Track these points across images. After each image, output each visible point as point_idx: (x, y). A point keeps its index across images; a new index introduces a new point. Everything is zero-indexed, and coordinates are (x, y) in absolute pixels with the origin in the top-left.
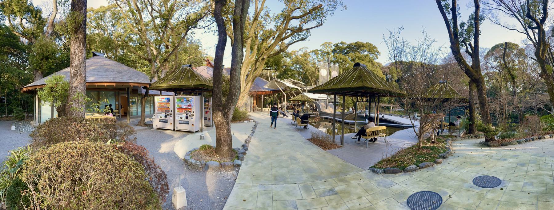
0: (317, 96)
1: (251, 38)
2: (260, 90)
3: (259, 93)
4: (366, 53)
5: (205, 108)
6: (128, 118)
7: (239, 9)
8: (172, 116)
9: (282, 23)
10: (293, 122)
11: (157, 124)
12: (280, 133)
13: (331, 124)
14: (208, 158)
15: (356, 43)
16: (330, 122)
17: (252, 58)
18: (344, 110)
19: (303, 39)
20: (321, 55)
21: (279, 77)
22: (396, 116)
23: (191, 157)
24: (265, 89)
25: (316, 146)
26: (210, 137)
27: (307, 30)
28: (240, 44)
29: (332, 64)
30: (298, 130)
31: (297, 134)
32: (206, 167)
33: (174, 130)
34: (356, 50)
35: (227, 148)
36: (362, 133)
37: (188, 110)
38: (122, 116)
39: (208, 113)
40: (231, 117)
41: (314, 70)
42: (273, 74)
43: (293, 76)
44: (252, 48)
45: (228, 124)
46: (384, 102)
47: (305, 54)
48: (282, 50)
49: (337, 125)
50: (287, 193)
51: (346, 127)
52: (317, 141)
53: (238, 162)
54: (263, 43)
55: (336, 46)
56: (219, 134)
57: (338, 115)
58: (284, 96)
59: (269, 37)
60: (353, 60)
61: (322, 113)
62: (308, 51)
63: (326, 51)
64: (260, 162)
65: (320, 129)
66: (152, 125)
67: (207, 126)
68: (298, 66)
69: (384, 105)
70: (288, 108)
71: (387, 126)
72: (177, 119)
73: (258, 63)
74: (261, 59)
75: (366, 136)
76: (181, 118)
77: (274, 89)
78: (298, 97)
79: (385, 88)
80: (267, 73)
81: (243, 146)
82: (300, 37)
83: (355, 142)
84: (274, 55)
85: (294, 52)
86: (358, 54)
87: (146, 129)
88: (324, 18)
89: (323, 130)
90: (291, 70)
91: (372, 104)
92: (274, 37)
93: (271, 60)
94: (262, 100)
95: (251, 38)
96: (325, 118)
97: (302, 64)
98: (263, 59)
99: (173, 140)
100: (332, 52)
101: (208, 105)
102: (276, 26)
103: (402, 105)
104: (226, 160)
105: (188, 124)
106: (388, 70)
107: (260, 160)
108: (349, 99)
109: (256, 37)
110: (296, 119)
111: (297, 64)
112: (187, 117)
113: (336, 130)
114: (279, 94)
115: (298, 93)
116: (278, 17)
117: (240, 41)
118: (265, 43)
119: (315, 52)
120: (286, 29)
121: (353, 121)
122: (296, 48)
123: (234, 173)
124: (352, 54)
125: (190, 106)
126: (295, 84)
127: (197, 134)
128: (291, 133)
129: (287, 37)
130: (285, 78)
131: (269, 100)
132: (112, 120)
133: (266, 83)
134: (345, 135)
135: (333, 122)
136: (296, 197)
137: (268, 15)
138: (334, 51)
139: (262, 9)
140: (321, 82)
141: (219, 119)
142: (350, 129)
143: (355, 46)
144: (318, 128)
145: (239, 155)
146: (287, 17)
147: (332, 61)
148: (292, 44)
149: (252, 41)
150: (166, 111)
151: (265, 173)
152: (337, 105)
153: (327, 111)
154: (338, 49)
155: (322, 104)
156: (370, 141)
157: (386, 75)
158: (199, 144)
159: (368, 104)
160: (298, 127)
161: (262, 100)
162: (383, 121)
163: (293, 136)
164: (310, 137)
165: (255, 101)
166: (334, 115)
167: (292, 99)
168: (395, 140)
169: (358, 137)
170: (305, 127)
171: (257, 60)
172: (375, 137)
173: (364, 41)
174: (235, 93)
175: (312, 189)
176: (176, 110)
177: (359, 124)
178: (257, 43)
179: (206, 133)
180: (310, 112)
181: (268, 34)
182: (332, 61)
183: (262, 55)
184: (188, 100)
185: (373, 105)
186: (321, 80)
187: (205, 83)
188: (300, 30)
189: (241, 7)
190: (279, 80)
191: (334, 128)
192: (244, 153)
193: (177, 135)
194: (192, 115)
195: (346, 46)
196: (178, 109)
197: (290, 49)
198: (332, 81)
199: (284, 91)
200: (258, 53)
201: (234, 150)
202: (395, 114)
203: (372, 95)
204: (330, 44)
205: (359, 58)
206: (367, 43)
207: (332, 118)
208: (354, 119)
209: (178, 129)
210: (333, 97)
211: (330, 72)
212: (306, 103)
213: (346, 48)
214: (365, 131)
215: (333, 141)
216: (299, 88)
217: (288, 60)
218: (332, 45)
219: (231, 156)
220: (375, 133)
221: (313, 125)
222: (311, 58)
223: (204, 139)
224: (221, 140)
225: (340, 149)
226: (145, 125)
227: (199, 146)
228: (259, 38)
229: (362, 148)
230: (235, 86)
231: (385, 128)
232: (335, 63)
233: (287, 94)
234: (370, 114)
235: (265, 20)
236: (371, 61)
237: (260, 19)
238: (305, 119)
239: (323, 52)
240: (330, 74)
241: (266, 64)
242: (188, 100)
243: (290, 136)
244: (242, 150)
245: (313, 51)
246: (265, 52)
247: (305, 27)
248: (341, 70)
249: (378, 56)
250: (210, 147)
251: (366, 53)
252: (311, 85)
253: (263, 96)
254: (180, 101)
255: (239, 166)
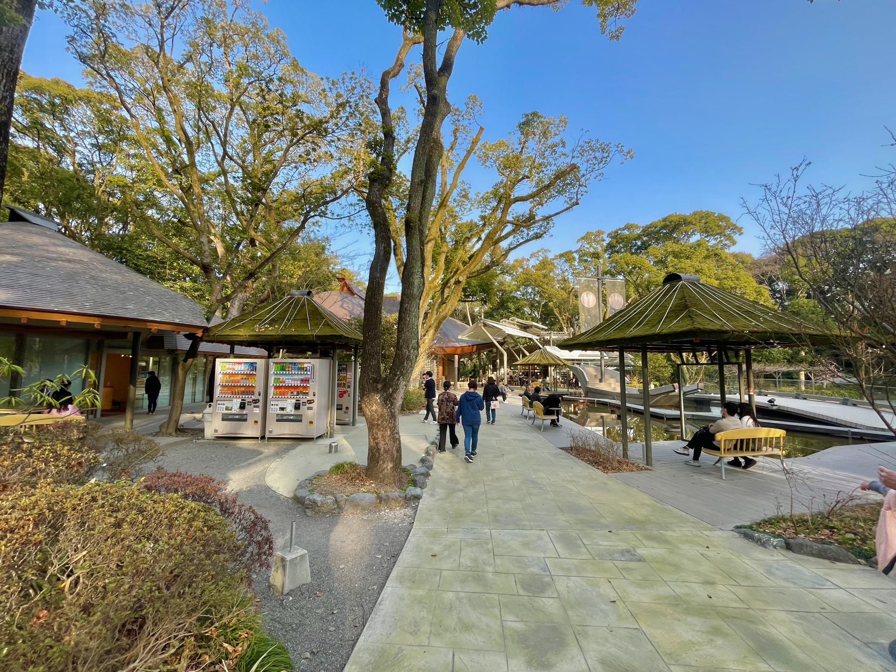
0: (576, 354)
1: (433, 242)
2: (451, 344)
3: (448, 351)
4: (695, 239)
5: (339, 385)
6: (129, 415)
7: (417, 201)
8: (260, 404)
9: (494, 210)
10: (526, 411)
11: (214, 426)
12: (498, 436)
13: (614, 416)
14: (350, 489)
15: (664, 220)
16: (613, 412)
17: (434, 279)
18: (646, 385)
19: (538, 236)
20: (581, 261)
21: (489, 315)
22: (823, 400)
23: (312, 492)
24: (462, 341)
25: (584, 463)
26: (353, 447)
27: (547, 218)
28: (419, 264)
29: (608, 279)
30: (539, 428)
31: (537, 438)
32: (336, 512)
33: (263, 438)
34: (668, 237)
35: (390, 465)
36: (704, 440)
37: (301, 390)
38: (105, 413)
39: (346, 395)
40: (399, 402)
41: (565, 295)
42: (477, 309)
43: (518, 311)
44: (435, 261)
45: (393, 416)
46: (770, 360)
47: (544, 264)
48: (494, 263)
49: (632, 420)
50: (526, 545)
51: (655, 424)
52: (581, 451)
53: (413, 491)
54: (456, 249)
55: (615, 236)
56: (375, 439)
57: (632, 396)
58: (502, 355)
59: (468, 239)
60: (661, 262)
61: (589, 392)
62: (551, 256)
63: (592, 250)
64: (461, 491)
65: (589, 428)
66: (203, 430)
67: (341, 423)
68: (530, 290)
69: (770, 368)
70: (511, 381)
71: (788, 429)
72: (274, 410)
73: (447, 291)
74: (453, 281)
75: (718, 449)
76: (282, 409)
77: (480, 341)
78: (533, 357)
79: (763, 327)
80: (465, 308)
81: (423, 461)
82: (531, 233)
83: (687, 463)
84: (479, 273)
85: (520, 263)
86: (670, 246)
87: (182, 442)
88: (582, 189)
89: (599, 430)
90: (515, 300)
91: (726, 368)
92: (480, 239)
93: (474, 282)
94: (456, 365)
95: (433, 242)
96: (599, 403)
97: (539, 286)
98: (458, 282)
99: (260, 460)
100: (606, 251)
101: (345, 378)
102: (483, 218)
103: (849, 366)
104: (389, 489)
105: (301, 421)
106: (775, 270)
107: (460, 487)
108: (657, 359)
109: (443, 239)
110: (531, 405)
111: (527, 286)
112: (297, 407)
113: (631, 433)
114: (491, 351)
115: (532, 348)
116: (486, 199)
117: (419, 258)
118: (461, 252)
119: (567, 256)
120: (503, 223)
121: (677, 413)
122: (524, 255)
123: (409, 511)
124: (657, 249)
125: (307, 381)
126: (525, 328)
127: (321, 442)
128: (523, 436)
129: (506, 237)
130: (502, 317)
131: (470, 365)
132: (78, 425)
133: (462, 330)
134: (654, 443)
135: (622, 412)
136: (545, 552)
137: (465, 196)
138: (610, 246)
139: (454, 186)
140: (586, 324)
141: (374, 408)
142: (666, 431)
143: (664, 227)
144: (584, 424)
145: (417, 478)
146: (504, 199)
147: (606, 273)
148: (515, 248)
149: (436, 245)
150: (243, 393)
151: (474, 511)
152: (629, 372)
153: (603, 387)
154: (619, 243)
155: (589, 372)
156: (730, 463)
157: (771, 282)
158: (327, 463)
159: (716, 367)
160: (537, 422)
161: (456, 365)
162: (768, 414)
163: (527, 441)
164: (568, 443)
165: (441, 368)
166: (623, 395)
167: (520, 360)
168: (820, 470)
169: (692, 451)
170: (554, 423)
171: (445, 284)
172: (749, 455)
173: (685, 210)
174: (409, 357)
175: (580, 542)
176: (271, 391)
177: (692, 420)
178: (445, 249)
179: (340, 439)
180: (562, 389)
181: (465, 230)
182: (606, 273)
183: (456, 273)
184: (302, 369)
185: (730, 371)
186: (582, 317)
187: (341, 333)
188: (530, 220)
189: (420, 198)
190: (490, 322)
191: (625, 427)
192: (427, 475)
193: (269, 449)
194: (310, 402)
195: (638, 232)
196: (276, 387)
197: (511, 258)
198: (608, 323)
199: (501, 344)
200: (447, 269)
201: (404, 470)
202: (820, 394)
203: (726, 347)
204: (600, 233)
205: (676, 255)
206: (695, 214)
207: (618, 402)
208: (678, 407)
209: (273, 435)
210: (616, 354)
211: (604, 296)
212: (551, 369)
213: (639, 237)
214: (712, 436)
215: (625, 455)
216: (535, 338)
217: (508, 278)
218: (605, 236)
219: (400, 481)
220: (741, 444)
221: (571, 419)
222: (558, 272)
223: (336, 451)
224: (379, 449)
225: (645, 474)
226: (181, 430)
227: (327, 467)
228: (448, 240)
229: (706, 479)
230: (407, 342)
231: (780, 433)
232: (613, 275)
233: (507, 350)
234: (723, 394)
235: (460, 205)
236: (715, 255)
237: (451, 203)
238: (552, 404)
239: (582, 254)
240: (605, 302)
241: (464, 290)
242: (302, 369)
243: (520, 440)
244: (420, 469)
245: (561, 256)
246: (462, 268)
247: (540, 213)
248: (632, 289)
249: (736, 237)
250: (353, 466)
251: (695, 239)
252: (561, 329)
253: (456, 357)
254: (283, 369)
255: (417, 498)
